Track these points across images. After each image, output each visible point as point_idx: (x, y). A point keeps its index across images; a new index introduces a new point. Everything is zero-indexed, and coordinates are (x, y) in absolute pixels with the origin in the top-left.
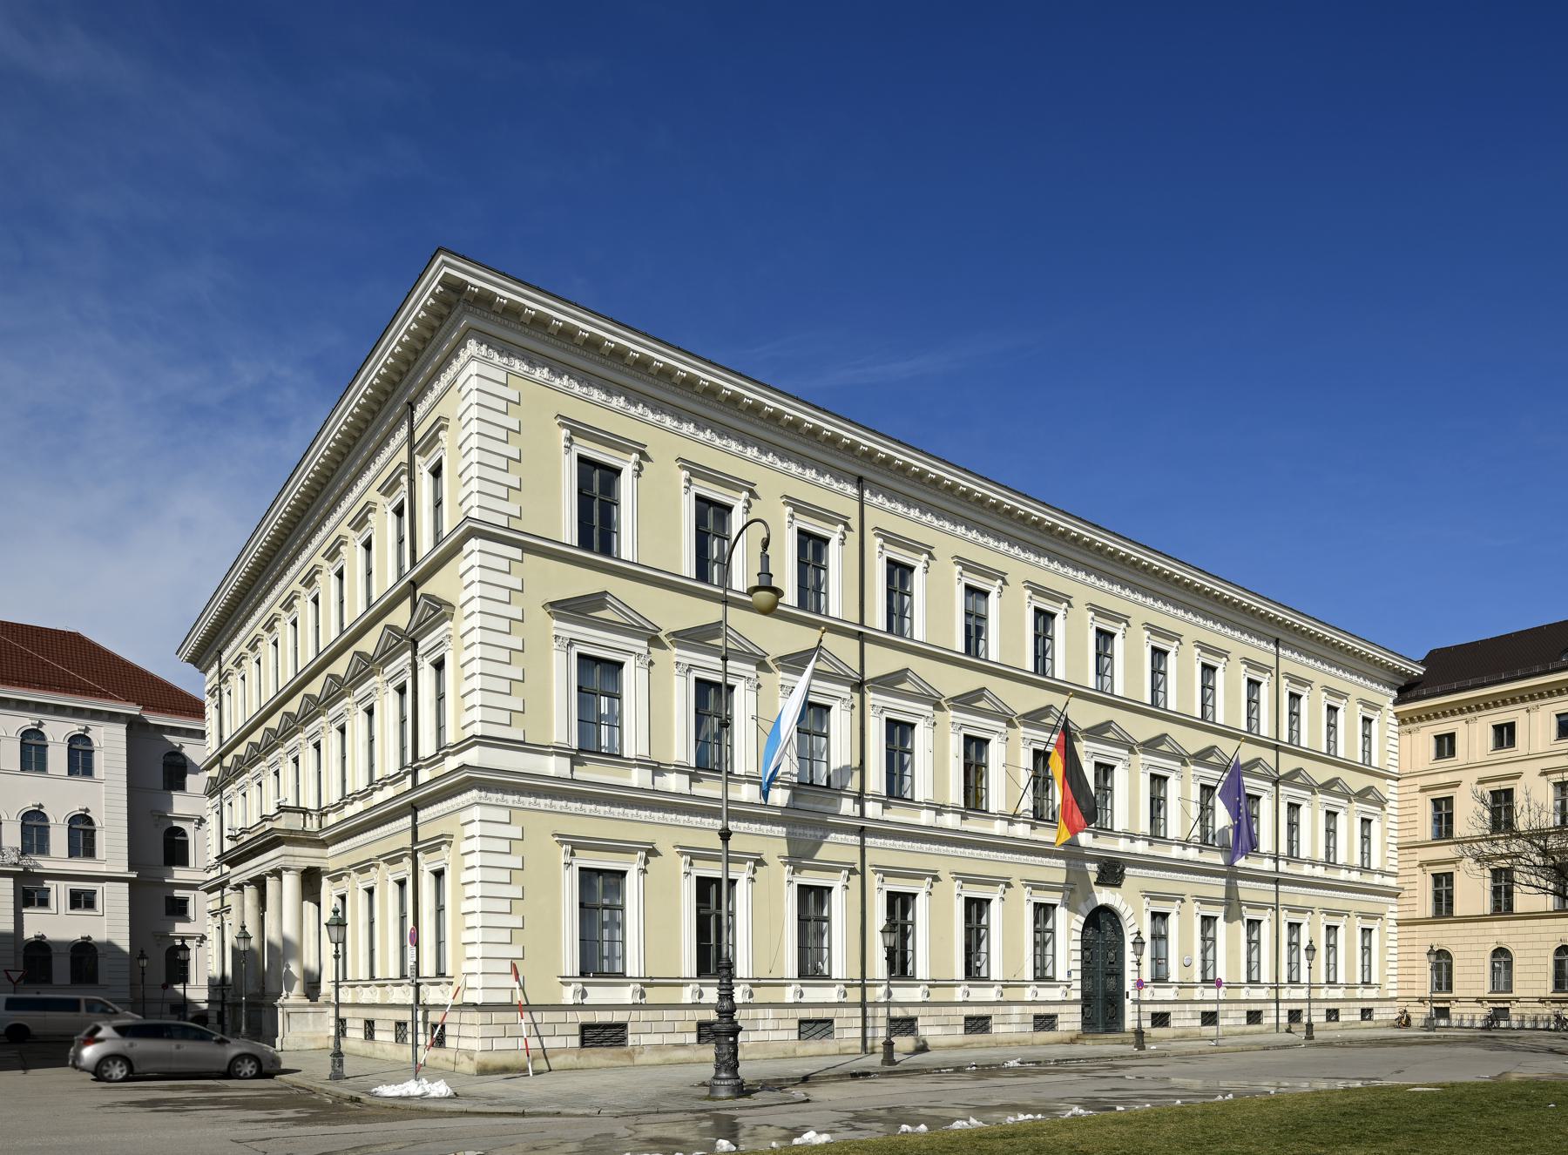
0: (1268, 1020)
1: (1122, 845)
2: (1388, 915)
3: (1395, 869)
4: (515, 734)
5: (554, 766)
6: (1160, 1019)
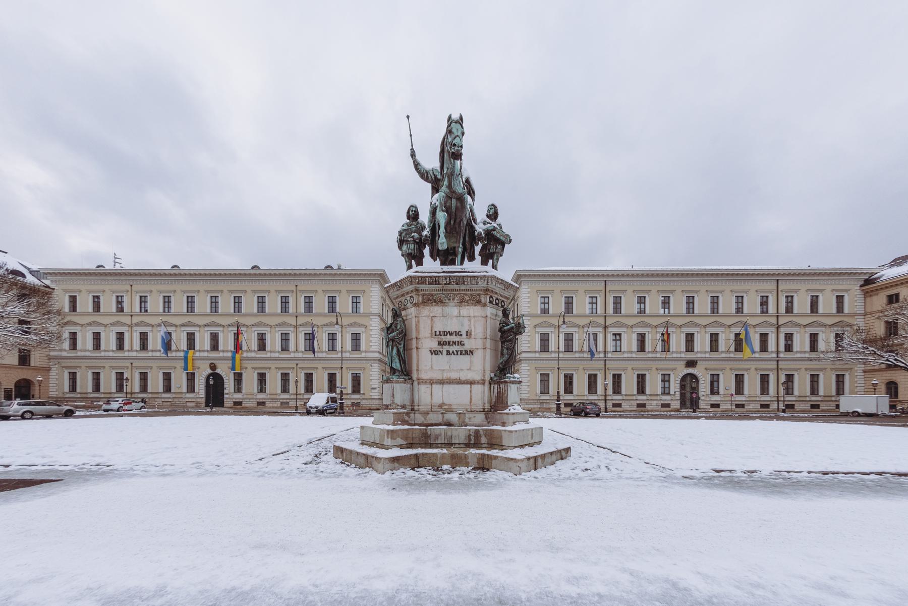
1: (699, 355)
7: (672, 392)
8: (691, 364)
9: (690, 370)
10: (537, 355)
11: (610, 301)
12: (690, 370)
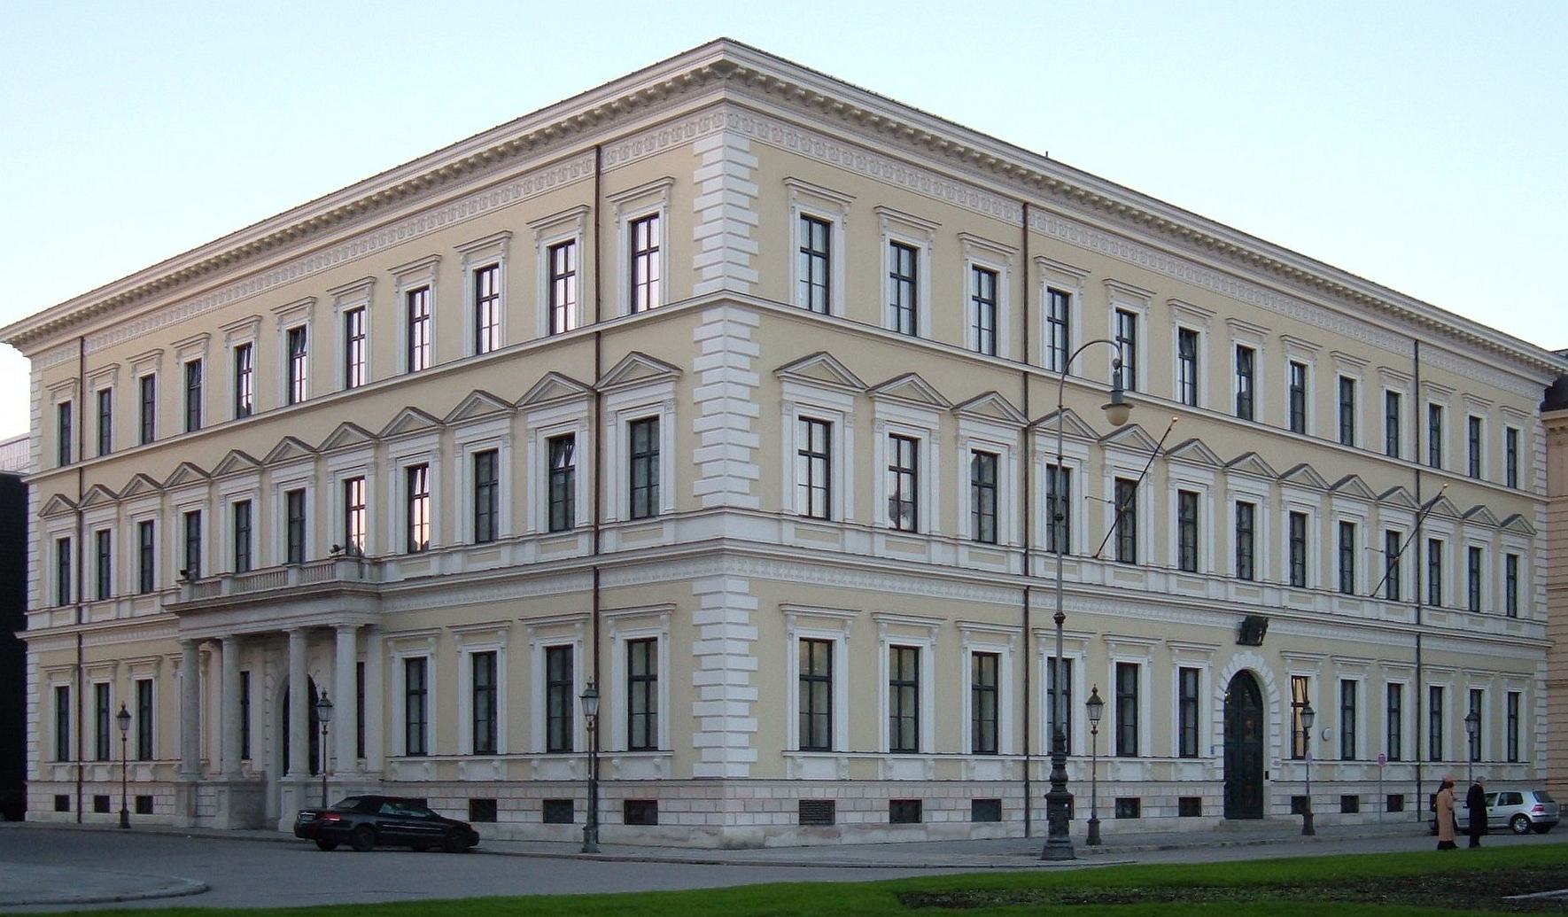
0: (1410, 807)
2: (1537, 676)
3: (1544, 618)
4: (752, 502)
5: (789, 534)
6: (1128, 807)
7: (1204, 750)
8: (1252, 631)
9: (1247, 659)
10: (789, 534)
11: (1042, 305)
12: (1247, 659)
